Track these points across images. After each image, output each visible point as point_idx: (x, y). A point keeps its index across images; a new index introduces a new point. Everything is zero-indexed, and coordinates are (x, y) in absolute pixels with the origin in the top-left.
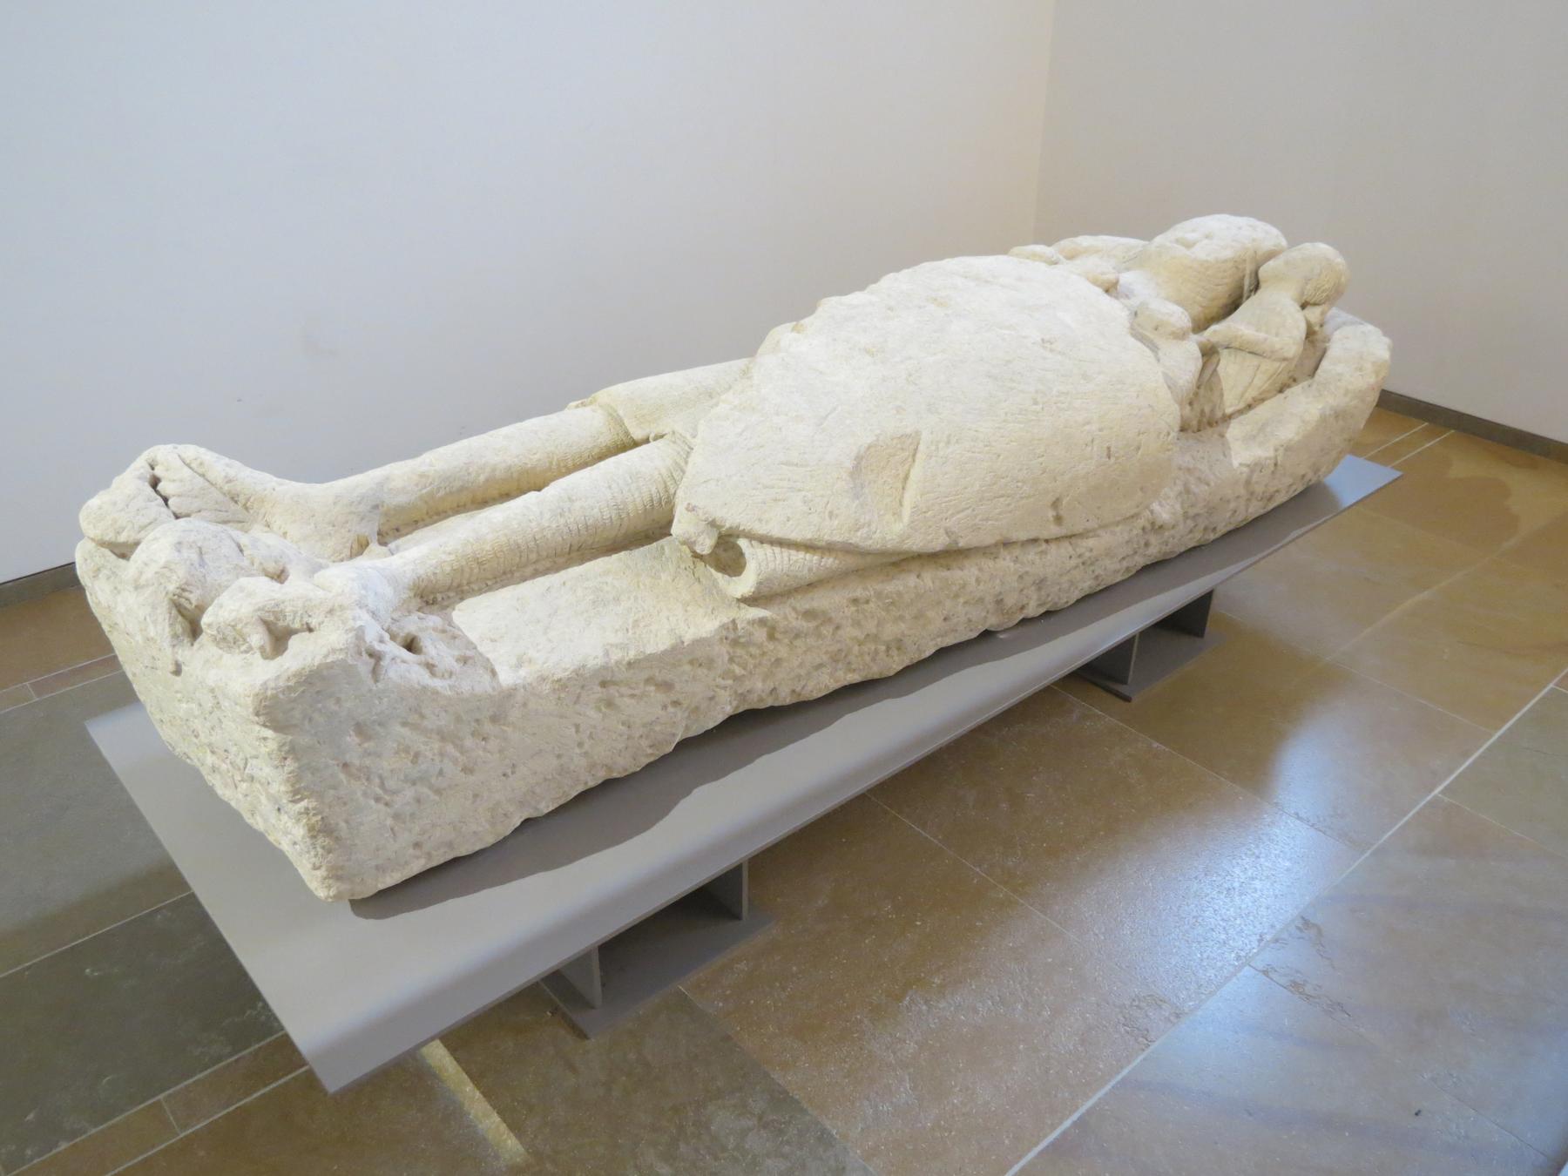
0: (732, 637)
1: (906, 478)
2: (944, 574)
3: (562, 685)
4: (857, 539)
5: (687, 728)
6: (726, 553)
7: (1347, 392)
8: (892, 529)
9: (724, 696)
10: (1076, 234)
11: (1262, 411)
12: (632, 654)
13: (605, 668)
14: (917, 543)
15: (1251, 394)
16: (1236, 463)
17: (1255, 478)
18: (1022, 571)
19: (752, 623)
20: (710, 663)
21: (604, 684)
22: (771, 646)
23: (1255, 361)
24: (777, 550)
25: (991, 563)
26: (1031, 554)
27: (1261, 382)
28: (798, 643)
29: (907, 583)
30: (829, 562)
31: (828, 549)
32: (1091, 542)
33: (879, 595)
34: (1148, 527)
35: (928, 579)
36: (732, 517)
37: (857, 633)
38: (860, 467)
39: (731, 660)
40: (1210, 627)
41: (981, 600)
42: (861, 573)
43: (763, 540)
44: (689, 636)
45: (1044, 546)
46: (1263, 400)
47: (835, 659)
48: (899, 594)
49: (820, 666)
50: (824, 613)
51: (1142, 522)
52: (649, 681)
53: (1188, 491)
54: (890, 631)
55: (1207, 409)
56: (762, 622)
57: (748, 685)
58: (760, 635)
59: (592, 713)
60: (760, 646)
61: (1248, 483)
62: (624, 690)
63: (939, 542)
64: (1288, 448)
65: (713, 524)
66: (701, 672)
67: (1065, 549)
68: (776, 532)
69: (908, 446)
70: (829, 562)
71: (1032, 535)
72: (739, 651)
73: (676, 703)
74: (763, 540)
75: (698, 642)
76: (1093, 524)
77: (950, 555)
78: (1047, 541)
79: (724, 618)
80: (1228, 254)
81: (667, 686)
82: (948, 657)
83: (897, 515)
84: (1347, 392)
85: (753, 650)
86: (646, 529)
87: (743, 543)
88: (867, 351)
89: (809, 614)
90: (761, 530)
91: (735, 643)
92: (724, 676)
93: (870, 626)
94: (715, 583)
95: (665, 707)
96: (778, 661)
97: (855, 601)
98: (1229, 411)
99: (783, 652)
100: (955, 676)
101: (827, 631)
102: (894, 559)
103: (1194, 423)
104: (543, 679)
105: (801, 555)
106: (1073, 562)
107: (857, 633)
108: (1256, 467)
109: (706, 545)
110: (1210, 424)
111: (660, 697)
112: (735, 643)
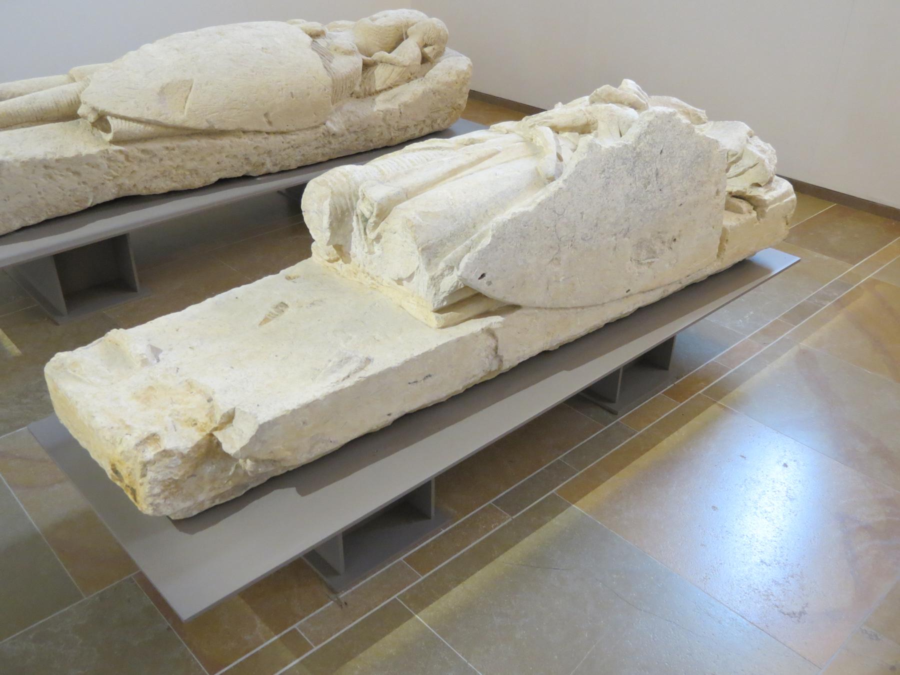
0: (105, 154)
1: (187, 98)
2: (212, 141)
3: (25, 164)
4: (161, 119)
5: (95, 197)
6: (101, 121)
7: (438, 83)
8: (178, 116)
9: (110, 184)
10: (338, 20)
11: (395, 91)
12: (57, 157)
13: (44, 160)
14: (191, 124)
15: (389, 83)
16: (375, 110)
17: (388, 118)
18: (256, 145)
19: (116, 151)
20: (97, 166)
21: (46, 167)
22: (127, 164)
23: (391, 67)
24: (123, 121)
25: (237, 140)
26: (259, 138)
27: (394, 77)
28: (142, 164)
29: (193, 143)
30: (149, 129)
31: (148, 123)
32: (294, 137)
33: (178, 146)
34: (326, 133)
35: (204, 142)
36: (104, 106)
37: (171, 163)
38: (163, 92)
39: (109, 167)
40: (670, 368)
41: (235, 156)
42: (171, 137)
43: (117, 117)
44: (84, 152)
45: (266, 135)
46: (398, 85)
47: (163, 174)
48: (189, 148)
49: (156, 177)
50: (152, 151)
51: (322, 129)
52: (68, 169)
53: (349, 120)
54: (190, 165)
55: (367, 88)
56: (121, 152)
57: (120, 181)
58: (121, 158)
59: (43, 180)
60: (123, 163)
61: (384, 119)
62: (56, 171)
63: (204, 125)
64: (406, 105)
65: (94, 109)
66: (94, 170)
67: (280, 138)
68: (122, 113)
69: (188, 85)
70: (149, 129)
71: (258, 128)
72: (112, 164)
73: (84, 183)
74: (117, 117)
75: (89, 156)
76: (291, 128)
77: (211, 133)
78: (268, 133)
79: (102, 148)
80: (392, 23)
81: (77, 173)
82: (223, 182)
83: (183, 113)
84: (438, 83)
85: (120, 165)
86: (67, 114)
87: (109, 118)
88: (177, 50)
89: (143, 151)
90: (115, 112)
91: (109, 159)
92: (107, 174)
93: (178, 161)
94: (101, 137)
95: (79, 184)
96: (133, 172)
97: (167, 148)
98: (378, 89)
99: (136, 168)
100: (484, 410)
101: (156, 160)
102: (189, 132)
103: (362, 94)
104: (16, 161)
105: (135, 124)
106: (286, 145)
107: (171, 163)
108: (387, 112)
109: (92, 118)
110: (370, 95)
111: (75, 178)
112: (109, 159)
